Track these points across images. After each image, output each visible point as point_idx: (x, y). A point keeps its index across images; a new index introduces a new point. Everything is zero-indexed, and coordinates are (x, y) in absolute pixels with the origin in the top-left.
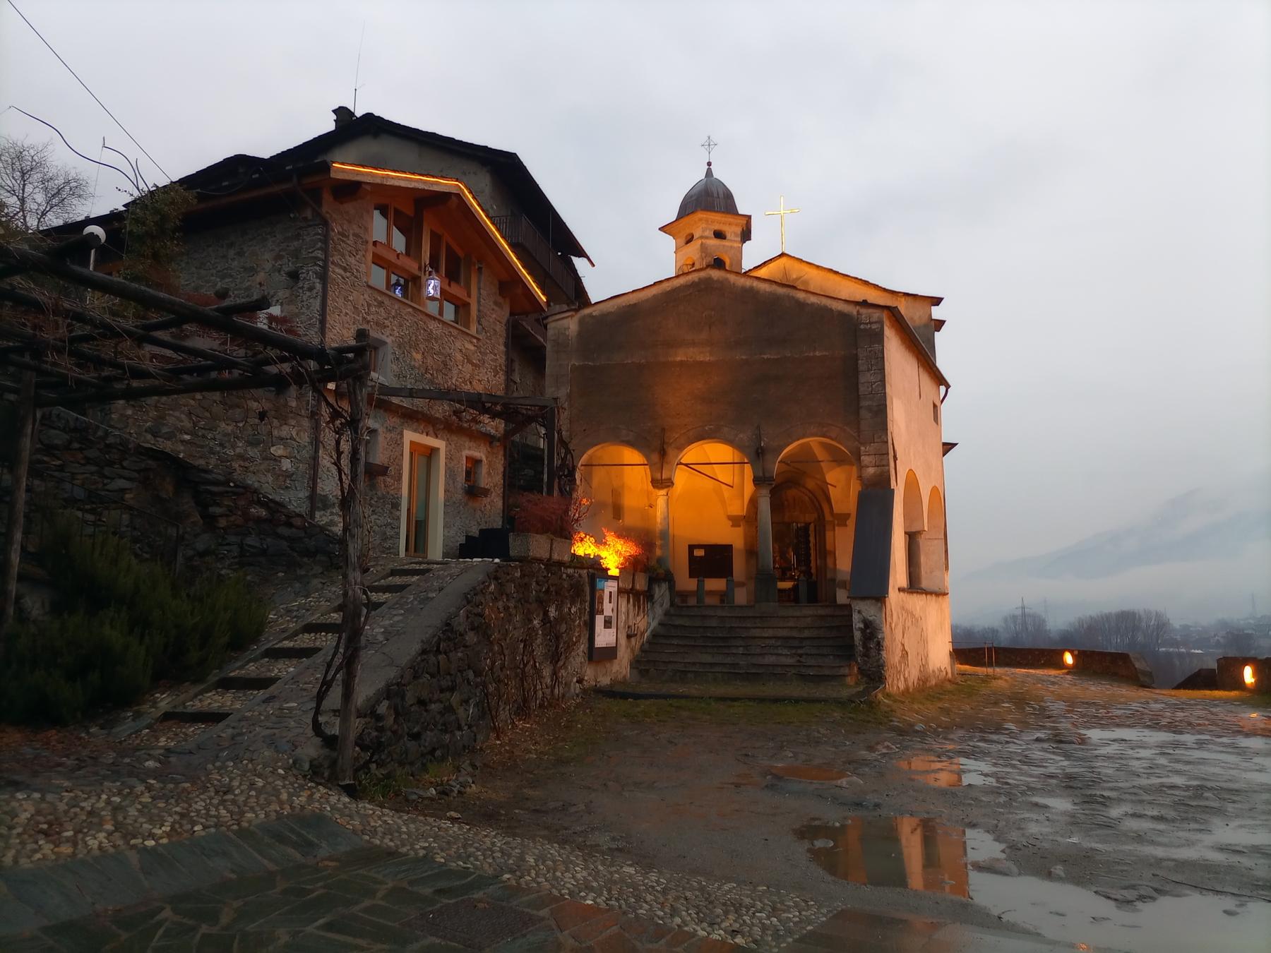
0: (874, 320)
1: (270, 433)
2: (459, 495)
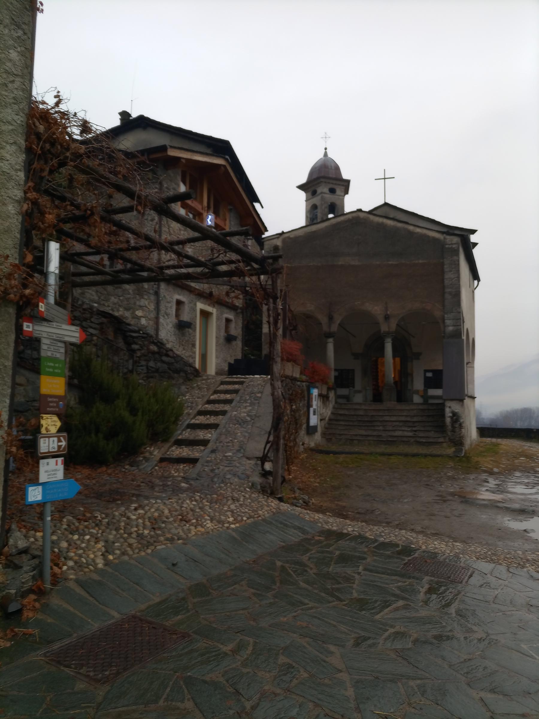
0: (454, 243)
1: (135, 304)
2: (222, 340)
